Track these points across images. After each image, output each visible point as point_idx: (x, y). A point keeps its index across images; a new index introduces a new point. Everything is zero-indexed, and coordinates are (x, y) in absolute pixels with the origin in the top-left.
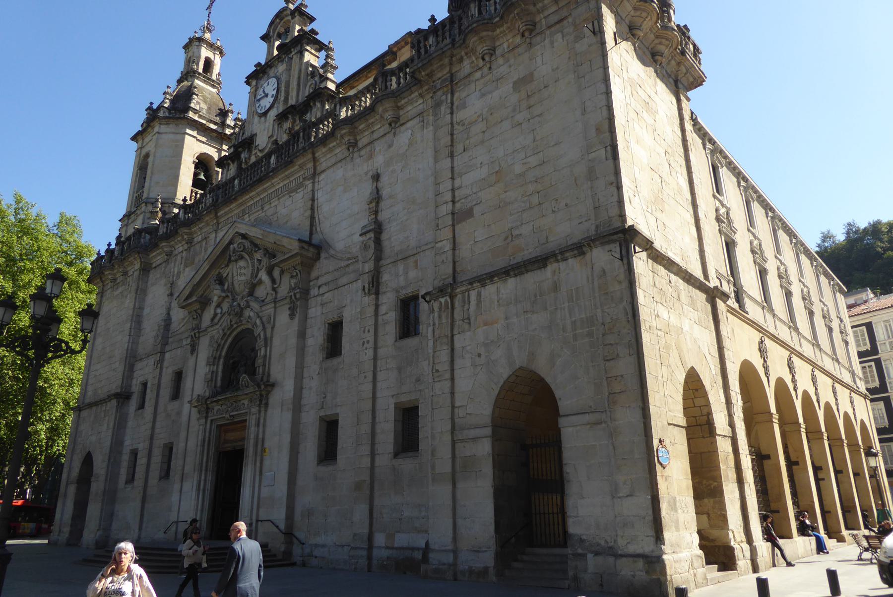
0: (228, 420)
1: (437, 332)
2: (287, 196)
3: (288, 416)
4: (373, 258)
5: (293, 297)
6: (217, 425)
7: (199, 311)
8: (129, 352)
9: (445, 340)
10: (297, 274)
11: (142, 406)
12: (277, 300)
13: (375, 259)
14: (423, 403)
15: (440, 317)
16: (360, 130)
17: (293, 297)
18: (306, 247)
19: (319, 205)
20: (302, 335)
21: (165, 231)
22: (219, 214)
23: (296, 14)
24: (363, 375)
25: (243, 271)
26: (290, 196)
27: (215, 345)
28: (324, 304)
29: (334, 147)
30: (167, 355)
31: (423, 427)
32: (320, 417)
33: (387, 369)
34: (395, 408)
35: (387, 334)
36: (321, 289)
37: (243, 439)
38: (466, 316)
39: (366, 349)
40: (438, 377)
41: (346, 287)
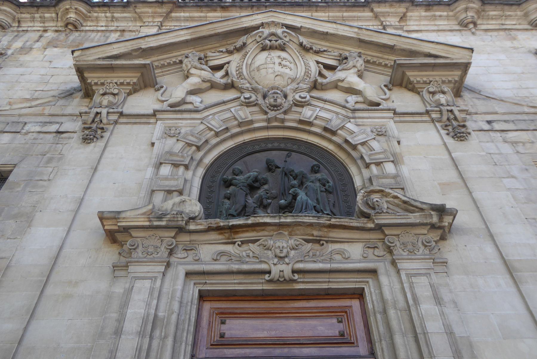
6: (364, 288)
8: (147, 190)
16: (488, 15)
19: (513, 33)
22: (173, 15)
29: (440, 16)
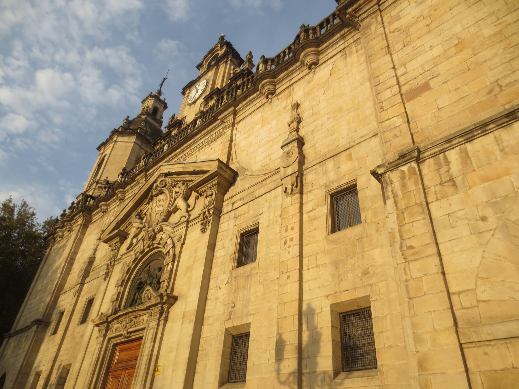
0: (125, 337)
1: (402, 204)
2: (208, 146)
3: (189, 328)
4: (297, 160)
5: (207, 213)
7: (118, 245)
9: (417, 209)
10: (212, 194)
11: (55, 333)
12: (189, 220)
13: (299, 162)
14: (377, 300)
15: (404, 186)
17: (207, 213)
18: (224, 169)
20: (212, 247)
21: (105, 194)
23: (224, 47)
24: (286, 275)
25: (161, 203)
26: (210, 146)
27: (126, 269)
28: (238, 216)
30: (86, 286)
31: (382, 332)
32: (226, 329)
33: (318, 266)
34: (332, 311)
35: (315, 230)
36: (235, 204)
37: (136, 359)
38: (445, 178)
39: (289, 247)
40: (414, 254)
41: (263, 197)
